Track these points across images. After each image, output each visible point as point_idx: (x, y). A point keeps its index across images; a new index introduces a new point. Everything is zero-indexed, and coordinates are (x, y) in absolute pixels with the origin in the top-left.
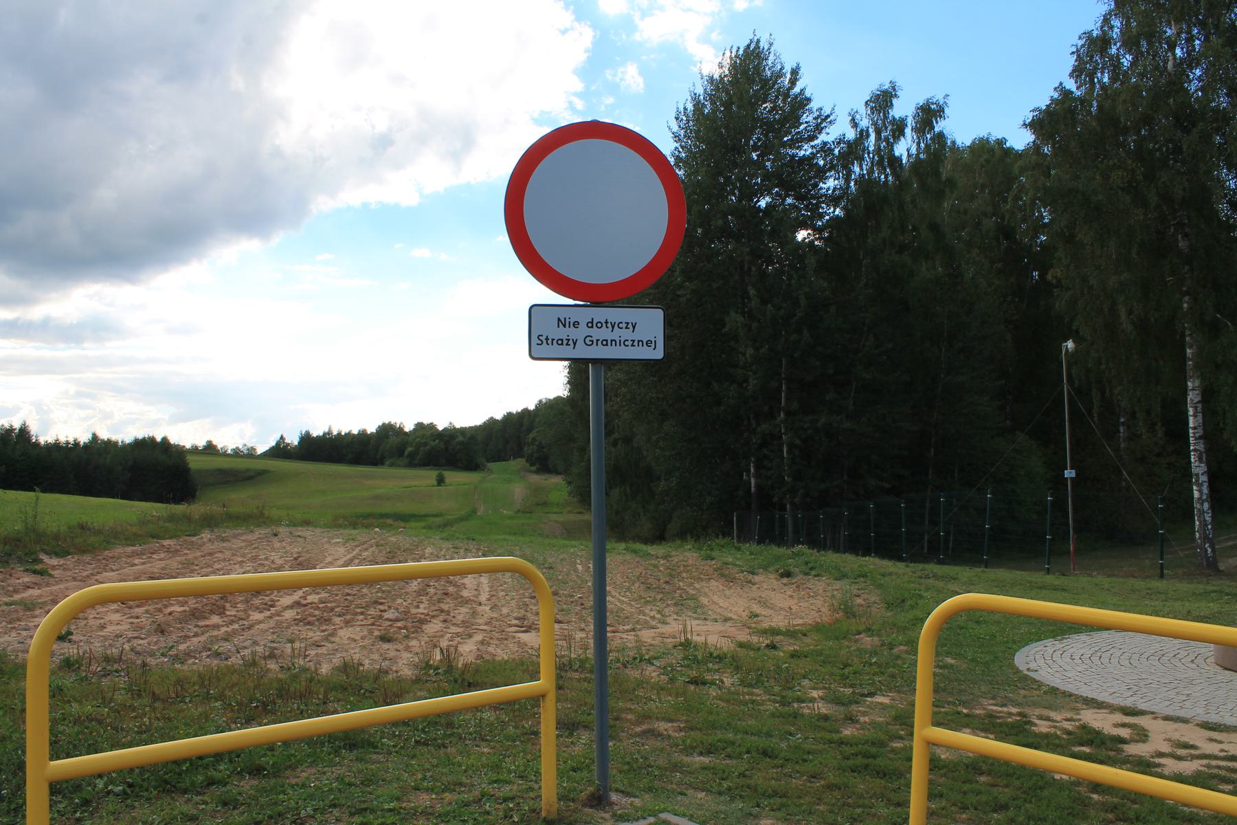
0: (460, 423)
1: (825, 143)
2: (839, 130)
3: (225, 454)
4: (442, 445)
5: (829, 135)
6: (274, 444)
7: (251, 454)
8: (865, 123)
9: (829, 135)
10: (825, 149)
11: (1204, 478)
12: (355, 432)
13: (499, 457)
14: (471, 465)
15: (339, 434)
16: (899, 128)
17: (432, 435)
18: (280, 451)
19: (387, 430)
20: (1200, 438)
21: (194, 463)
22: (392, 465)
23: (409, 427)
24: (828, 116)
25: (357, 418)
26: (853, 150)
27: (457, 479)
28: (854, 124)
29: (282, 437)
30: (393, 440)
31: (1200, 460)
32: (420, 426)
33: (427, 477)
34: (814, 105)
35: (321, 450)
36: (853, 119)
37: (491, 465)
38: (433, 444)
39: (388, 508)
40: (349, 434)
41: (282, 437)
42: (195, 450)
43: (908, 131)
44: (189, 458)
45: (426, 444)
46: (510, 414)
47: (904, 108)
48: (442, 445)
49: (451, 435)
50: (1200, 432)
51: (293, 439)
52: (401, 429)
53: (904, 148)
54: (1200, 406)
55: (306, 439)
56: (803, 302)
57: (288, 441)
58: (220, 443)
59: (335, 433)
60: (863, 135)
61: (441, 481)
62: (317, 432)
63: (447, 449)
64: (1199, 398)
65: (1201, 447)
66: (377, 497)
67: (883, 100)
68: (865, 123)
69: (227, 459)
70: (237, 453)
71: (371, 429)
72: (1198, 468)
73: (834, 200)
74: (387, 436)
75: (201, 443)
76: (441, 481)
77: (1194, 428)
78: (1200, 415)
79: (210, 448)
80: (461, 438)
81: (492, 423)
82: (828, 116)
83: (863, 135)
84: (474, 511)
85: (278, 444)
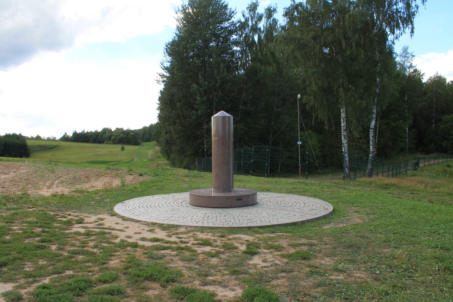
0: (133, 128)
1: (233, 21)
2: (237, 18)
3: (44, 140)
4: (125, 136)
5: (235, 19)
6: (62, 136)
7: (54, 140)
8: (247, 15)
9: (235, 19)
10: (233, 24)
11: (346, 145)
12: (93, 131)
13: (148, 140)
14: (136, 143)
15: (88, 132)
16: (260, 18)
17: (121, 132)
18: (65, 138)
19: (105, 131)
20: (345, 130)
21: (29, 143)
22: (107, 143)
23: (113, 129)
24: (233, 12)
25: (95, 127)
26: (243, 25)
27: (129, 148)
28: (244, 16)
29: (66, 133)
30: (108, 134)
31: (345, 138)
32: (118, 129)
33: (118, 147)
34: (229, 7)
35: (80, 138)
36: (243, 14)
37: (145, 144)
38: (121, 135)
39: (101, 159)
40: (91, 132)
41: (66, 133)
42: (32, 138)
43: (263, 18)
44: (27, 141)
45: (119, 136)
46: (152, 124)
47: (261, 10)
48: (125, 136)
49: (128, 132)
50: (345, 128)
51: (70, 134)
52: (111, 130)
53: (262, 25)
54: (345, 119)
55: (75, 134)
56: (218, 80)
57: (68, 135)
58: (42, 136)
59: (86, 132)
60: (247, 20)
61: (123, 149)
62: (79, 131)
63: (127, 137)
64: (345, 116)
65: (345, 133)
66: (97, 155)
67: (253, 7)
68: (247, 15)
69: (43, 141)
70: (49, 139)
71: (100, 130)
72: (344, 141)
73: (236, 43)
74: (105, 133)
75: (35, 136)
76: (123, 149)
77: (343, 127)
78: (345, 122)
79: (38, 138)
80: (132, 133)
81: (145, 128)
82: (233, 12)
83: (247, 20)
84: (133, 160)
85: (64, 136)
